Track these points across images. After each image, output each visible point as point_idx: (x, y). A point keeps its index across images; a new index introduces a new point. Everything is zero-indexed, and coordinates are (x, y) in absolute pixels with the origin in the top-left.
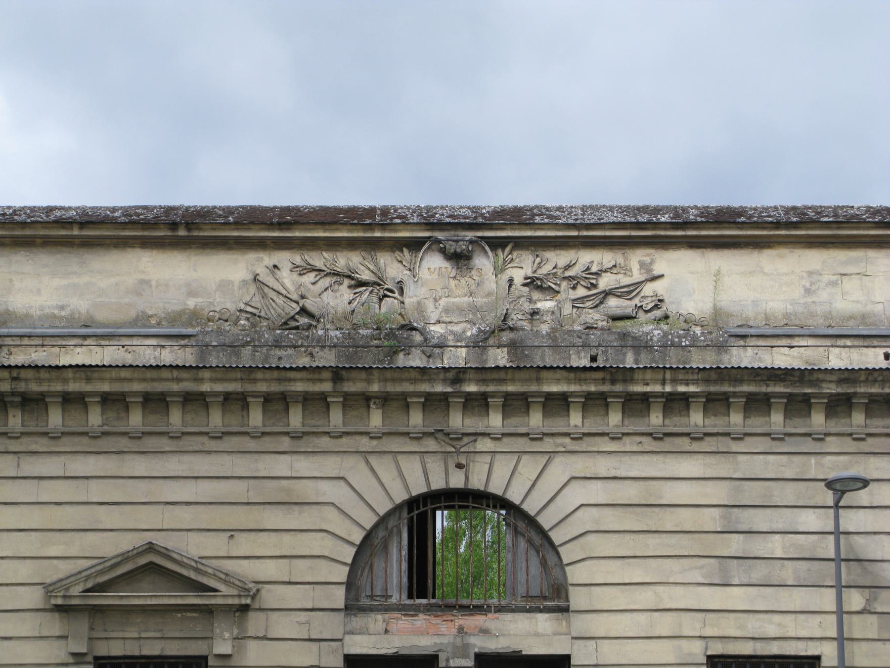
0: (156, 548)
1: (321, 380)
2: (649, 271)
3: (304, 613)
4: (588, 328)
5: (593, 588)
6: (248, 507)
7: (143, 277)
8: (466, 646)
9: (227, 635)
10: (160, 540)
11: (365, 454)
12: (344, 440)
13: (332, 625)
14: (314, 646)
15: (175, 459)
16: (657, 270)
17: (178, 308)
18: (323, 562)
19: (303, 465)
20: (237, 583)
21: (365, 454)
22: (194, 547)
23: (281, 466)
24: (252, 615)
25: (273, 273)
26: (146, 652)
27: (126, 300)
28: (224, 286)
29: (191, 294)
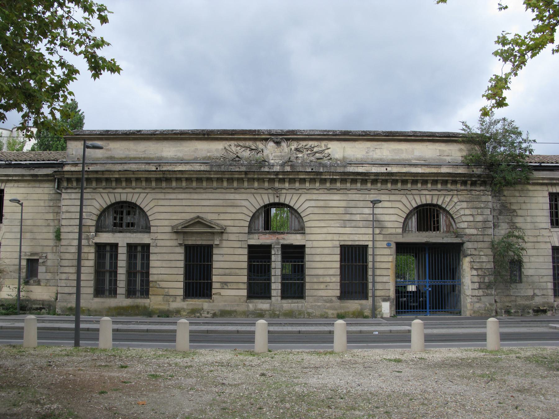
10: (201, 215)
19: (237, 196)
22: (209, 217)
23: (232, 196)
24: (224, 234)
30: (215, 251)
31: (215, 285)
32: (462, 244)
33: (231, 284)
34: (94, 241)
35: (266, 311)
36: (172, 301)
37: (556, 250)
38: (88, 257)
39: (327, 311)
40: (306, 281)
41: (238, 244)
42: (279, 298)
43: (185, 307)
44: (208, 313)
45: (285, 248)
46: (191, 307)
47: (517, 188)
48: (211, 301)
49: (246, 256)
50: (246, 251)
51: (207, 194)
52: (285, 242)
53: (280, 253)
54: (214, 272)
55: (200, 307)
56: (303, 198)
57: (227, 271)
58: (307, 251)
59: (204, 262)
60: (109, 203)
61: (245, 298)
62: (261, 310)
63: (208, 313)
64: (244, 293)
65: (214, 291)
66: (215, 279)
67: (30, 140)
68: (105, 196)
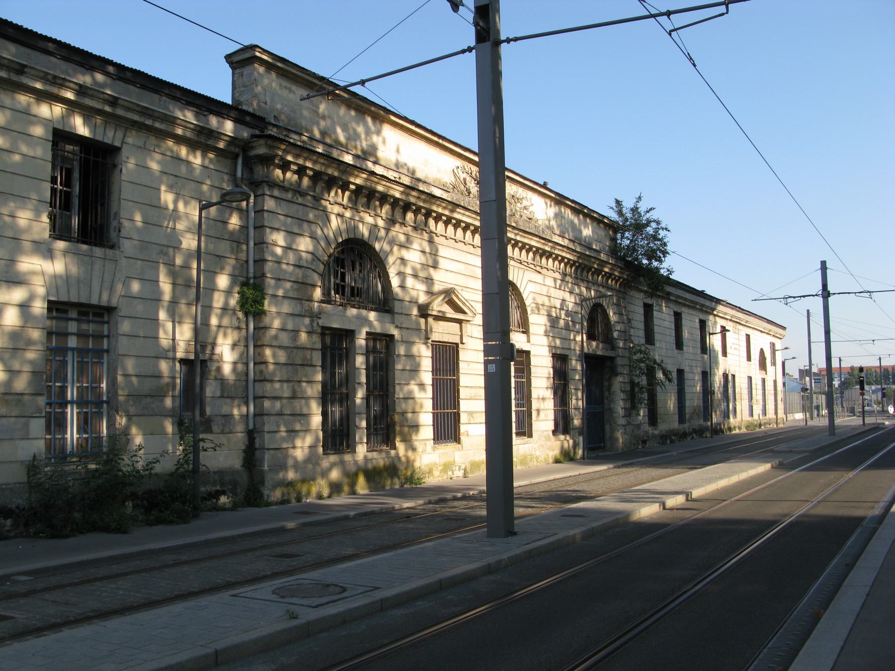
10: (456, 287)
15: (452, 250)
31: (463, 418)
32: (612, 359)
34: (321, 322)
40: (461, 409)
43: (437, 461)
46: (443, 460)
55: (452, 459)
65: (463, 428)
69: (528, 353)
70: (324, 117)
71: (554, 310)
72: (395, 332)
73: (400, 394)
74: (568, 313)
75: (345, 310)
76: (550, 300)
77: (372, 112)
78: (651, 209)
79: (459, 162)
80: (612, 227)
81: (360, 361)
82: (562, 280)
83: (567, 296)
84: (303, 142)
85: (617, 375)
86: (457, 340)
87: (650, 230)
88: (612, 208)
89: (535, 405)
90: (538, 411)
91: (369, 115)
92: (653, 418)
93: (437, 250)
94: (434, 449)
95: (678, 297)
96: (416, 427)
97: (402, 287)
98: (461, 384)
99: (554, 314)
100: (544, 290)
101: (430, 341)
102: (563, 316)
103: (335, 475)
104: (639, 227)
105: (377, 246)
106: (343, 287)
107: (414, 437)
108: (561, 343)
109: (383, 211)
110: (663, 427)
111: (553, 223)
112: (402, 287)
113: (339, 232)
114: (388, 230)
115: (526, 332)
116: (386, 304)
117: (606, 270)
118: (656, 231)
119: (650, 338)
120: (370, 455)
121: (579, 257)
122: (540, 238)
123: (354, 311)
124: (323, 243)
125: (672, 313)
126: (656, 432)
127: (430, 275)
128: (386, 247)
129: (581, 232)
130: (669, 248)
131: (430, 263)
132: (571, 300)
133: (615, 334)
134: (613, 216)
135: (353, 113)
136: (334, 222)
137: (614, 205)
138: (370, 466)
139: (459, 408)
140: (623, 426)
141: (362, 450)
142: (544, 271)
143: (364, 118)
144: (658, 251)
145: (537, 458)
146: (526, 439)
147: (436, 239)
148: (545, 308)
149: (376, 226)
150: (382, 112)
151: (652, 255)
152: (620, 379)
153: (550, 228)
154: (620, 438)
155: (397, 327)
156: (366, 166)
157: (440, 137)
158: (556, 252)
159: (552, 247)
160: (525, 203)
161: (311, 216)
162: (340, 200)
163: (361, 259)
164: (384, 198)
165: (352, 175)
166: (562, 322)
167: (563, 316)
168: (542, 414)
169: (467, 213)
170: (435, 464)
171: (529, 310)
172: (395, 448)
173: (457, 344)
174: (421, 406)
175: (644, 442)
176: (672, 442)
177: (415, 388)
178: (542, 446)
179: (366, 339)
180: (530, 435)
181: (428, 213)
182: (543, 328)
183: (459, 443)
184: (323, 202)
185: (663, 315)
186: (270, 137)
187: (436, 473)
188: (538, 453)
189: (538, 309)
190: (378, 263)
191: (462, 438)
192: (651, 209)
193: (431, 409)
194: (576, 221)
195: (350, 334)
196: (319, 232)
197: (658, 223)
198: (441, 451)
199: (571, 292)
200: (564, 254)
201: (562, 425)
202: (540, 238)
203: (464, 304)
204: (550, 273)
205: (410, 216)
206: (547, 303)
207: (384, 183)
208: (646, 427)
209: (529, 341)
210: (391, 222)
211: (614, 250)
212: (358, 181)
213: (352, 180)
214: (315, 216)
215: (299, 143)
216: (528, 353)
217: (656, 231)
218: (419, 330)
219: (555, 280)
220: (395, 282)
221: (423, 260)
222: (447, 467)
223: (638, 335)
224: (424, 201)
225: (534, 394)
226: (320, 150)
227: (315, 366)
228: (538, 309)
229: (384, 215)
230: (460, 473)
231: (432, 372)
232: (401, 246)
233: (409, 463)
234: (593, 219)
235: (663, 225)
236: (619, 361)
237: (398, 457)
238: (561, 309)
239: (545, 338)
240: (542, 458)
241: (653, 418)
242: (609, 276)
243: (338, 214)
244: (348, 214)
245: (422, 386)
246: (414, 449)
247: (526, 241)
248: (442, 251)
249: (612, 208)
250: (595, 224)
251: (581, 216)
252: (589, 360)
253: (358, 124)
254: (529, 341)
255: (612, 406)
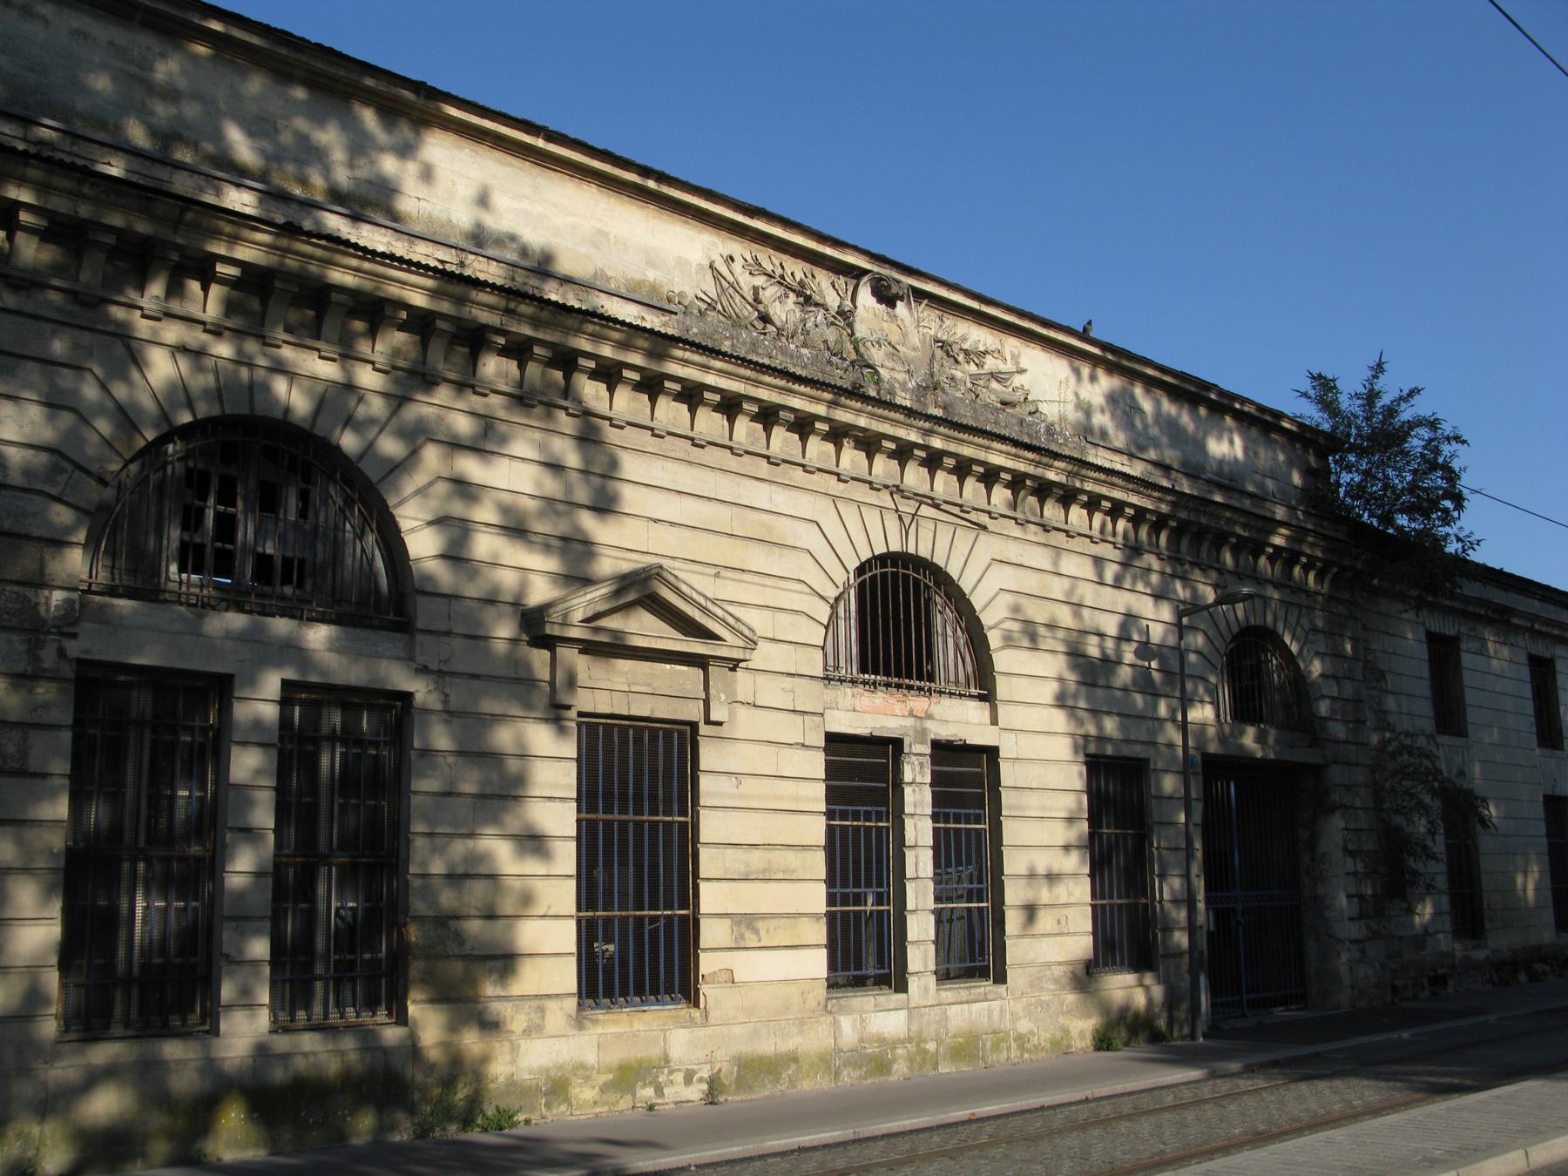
0: (665, 575)
1: (819, 400)
2: (1017, 363)
3: (789, 679)
4: (1003, 403)
5: (1014, 680)
6: (732, 540)
7: (599, 226)
8: (924, 731)
9: (723, 697)
10: (666, 563)
11: (835, 498)
12: (817, 477)
13: (811, 695)
14: (798, 719)
15: (658, 463)
16: (1024, 364)
17: (638, 277)
18: (804, 619)
19: (781, 500)
20: (746, 632)
21: (835, 498)
22: (699, 583)
23: (760, 495)
24: (740, 673)
25: (726, 261)
26: (636, 711)
27: (584, 250)
28: (681, 263)
29: (651, 263)
30: (709, 756)
31: (711, 933)
32: (1316, 770)
33: (773, 923)
34: (74, 648)
35: (895, 1043)
36: (527, 1032)
37: (1554, 804)
38: (23, 754)
39: (1067, 1022)
40: (704, 907)
41: (790, 729)
42: (932, 979)
43: (591, 1058)
44: (689, 1078)
45: (944, 751)
46: (615, 1056)
47: (1512, 639)
48: (696, 1013)
49: (820, 789)
50: (816, 764)
51: (670, 465)
52: (945, 733)
53: (928, 779)
54: (709, 863)
55: (655, 1052)
56: (988, 546)
57: (756, 859)
58: (1008, 774)
59: (638, 812)
60: (880, 549)
61: (821, 990)
62: (881, 1041)
63: (689, 1078)
64: (816, 963)
65: (708, 963)
66: (711, 898)
67: (1093, 378)
68: (872, 518)
69: (992, 753)
70: (171, 94)
71: (1094, 640)
72: (421, 690)
73: (429, 861)
74: (1145, 650)
75: (201, 617)
76: (1077, 615)
77: (367, 90)
78: (1412, 393)
79: (739, 248)
80: (1304, 437)
81: (246, 764)
82: (1125, 565)
83: (1145, 606)
84: (41, 142)
85: (1331, 810)
86: (693, 712)
87: (1415, 443)
88: (1305, 395)
89: (1014, 894)
90: (1031, 911)
91: (367, 103)
92: (1468, 912)
93: (614, 464)
94: (579, 1023)
95: (1536, 618)
96: (505, 961)
97: (455, 555)
98: (705, 836)
99: (1093, 651)
100: (1057, 588)
101: (573, 714)
102: (1129, 657)
103: (105, 1105)
104: (1387, 437)
105: (349, 442)
106: (230, 555)
107: (490, 989)
108: (1123, 728)
109: (378, 347)
110: (1500, 941)
111: (1101, 420)
112: (455, 555)
113: (181, 394)
114: (398, 400)
115: (987, 695)
116: (391, 605)
117: (1278, 541)
118: (1432, 447)
119: (1449, 713)
120: (282, 1043)
121: (1174, 504)
122: (1016, 443)
123: (236, 621)
124: (104, 426)
125: (1523, 659)
126: (1480, 955)
127: (578, 529)
128: (390, 446)
129: (1202, 448)
130: (1465, 482)
131: (582, 495)
132: (1157, 619)
133: (1324, 708)
134: (1310, 413)
135: (300, 93)
136: (162, 368)
137: (1306, 385)
138: (278, 1075)
139: (697, 905)
140: (1357, 941)
141: (245, 1030)
142: (1059, 539)
143: (349, 109)
144: (1440, 491)
145: (1021, 1040)
146: (985, 987)
147: (611, 435)
148: (1061, 634)
149: (350, 387)
150: (408, 95)
151: (1425, 505)
152: (1338, 822)
153: (1086, 431)
154: (1349, 969)
155: (423, 670)
156: (318, 222)
157: (646, 172)
158: (1089, 486)
159: (1070, 474)
160: (990, 363)
161: (59, 347)
162: (194, 310)
163: (307, 478)
164: (375, 311)
165: (216, 234)
166: (1124, 674)
167: (1129, 657)
168: (1045, 921)
169: (718, 364)
170: (582, 1066)
171: (994, 639)
172: (402, 1018)
173: (694, 726)
174: (527, 899)
175: (1439, 981)
176: (1534, 977)
177: (501, 852)
178: (1045, 1006)
179: (285, 702)
180: (1001, 978)
181: (567, 360)
182: (1054, 687)
183: (697, 1005)
184: (118, 313)
185: (1495, 666)
186: (856, 350)
187: (585, 1094)
188: (1024, 1026)
189: (1033, 637)
190: (367, 493)
191: (704, 989)
192: (1412, 393)
193: (571, 908)
194: (1185, 419)
195: (220, 688)
196: (90, 392)
197: (1433, 424)
198: (612, 1029)
199: (1158, 596)
200: (1117, 494)
201: (1124, 936)
202: (1016, 443)
203: (704, 610)
204: (1079, 544)
205: (493, 367)
206: (1065, 616)
207: (354, 262)
208: (1444, 942)
209: (994, 721)
210: (413, 379)
211: (1319, 498)
212: (244, 253)
213: (220, 249)
214: (76, 346)
215: (21, 146)
216: (992, 753)
217: (1432, 447)
218: (530, 682)
219: (1098, 561)
220: (422, 544)
221: (551, 486)
222: (628, 1076)
223: (1411, 704)
224: (535, 323)
225: (1014, 863)
226: (114, 171)
227: (44, 775)
228: (1033, 637)
229: (380, 359)
230: (695, 1092)
231: (578, 800)
232: (455, 445)
233: (457, 1068)
234: (1240, 416)
235: (1446, 428)
236: (1336, 775)
237: (413, 1049)
238: (1123, 637)
239: (1059, 720)
240: (1044, 1036)
241: (1468, 912)
242: (1288, 557)
243: (172, 348)
244: (223, 349)
245: (533, 842)
246: (490, 1026)
247: (967, 451)
248: (631, 466)
249: (1305, 395)
250: (1254, 432)
251: (1203, 411)
252: (1215, 768)
253: (320, 121)
254: (994, 721)
255: (1321, 891)
